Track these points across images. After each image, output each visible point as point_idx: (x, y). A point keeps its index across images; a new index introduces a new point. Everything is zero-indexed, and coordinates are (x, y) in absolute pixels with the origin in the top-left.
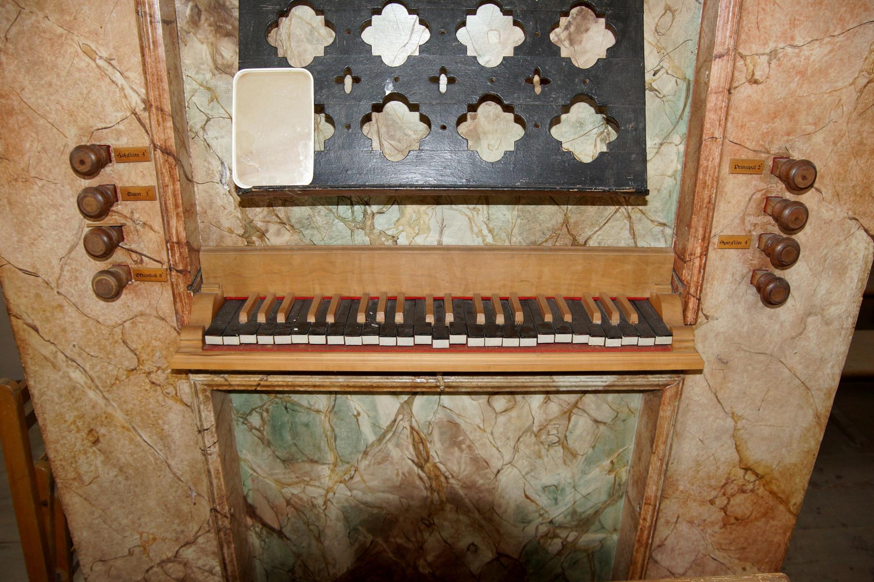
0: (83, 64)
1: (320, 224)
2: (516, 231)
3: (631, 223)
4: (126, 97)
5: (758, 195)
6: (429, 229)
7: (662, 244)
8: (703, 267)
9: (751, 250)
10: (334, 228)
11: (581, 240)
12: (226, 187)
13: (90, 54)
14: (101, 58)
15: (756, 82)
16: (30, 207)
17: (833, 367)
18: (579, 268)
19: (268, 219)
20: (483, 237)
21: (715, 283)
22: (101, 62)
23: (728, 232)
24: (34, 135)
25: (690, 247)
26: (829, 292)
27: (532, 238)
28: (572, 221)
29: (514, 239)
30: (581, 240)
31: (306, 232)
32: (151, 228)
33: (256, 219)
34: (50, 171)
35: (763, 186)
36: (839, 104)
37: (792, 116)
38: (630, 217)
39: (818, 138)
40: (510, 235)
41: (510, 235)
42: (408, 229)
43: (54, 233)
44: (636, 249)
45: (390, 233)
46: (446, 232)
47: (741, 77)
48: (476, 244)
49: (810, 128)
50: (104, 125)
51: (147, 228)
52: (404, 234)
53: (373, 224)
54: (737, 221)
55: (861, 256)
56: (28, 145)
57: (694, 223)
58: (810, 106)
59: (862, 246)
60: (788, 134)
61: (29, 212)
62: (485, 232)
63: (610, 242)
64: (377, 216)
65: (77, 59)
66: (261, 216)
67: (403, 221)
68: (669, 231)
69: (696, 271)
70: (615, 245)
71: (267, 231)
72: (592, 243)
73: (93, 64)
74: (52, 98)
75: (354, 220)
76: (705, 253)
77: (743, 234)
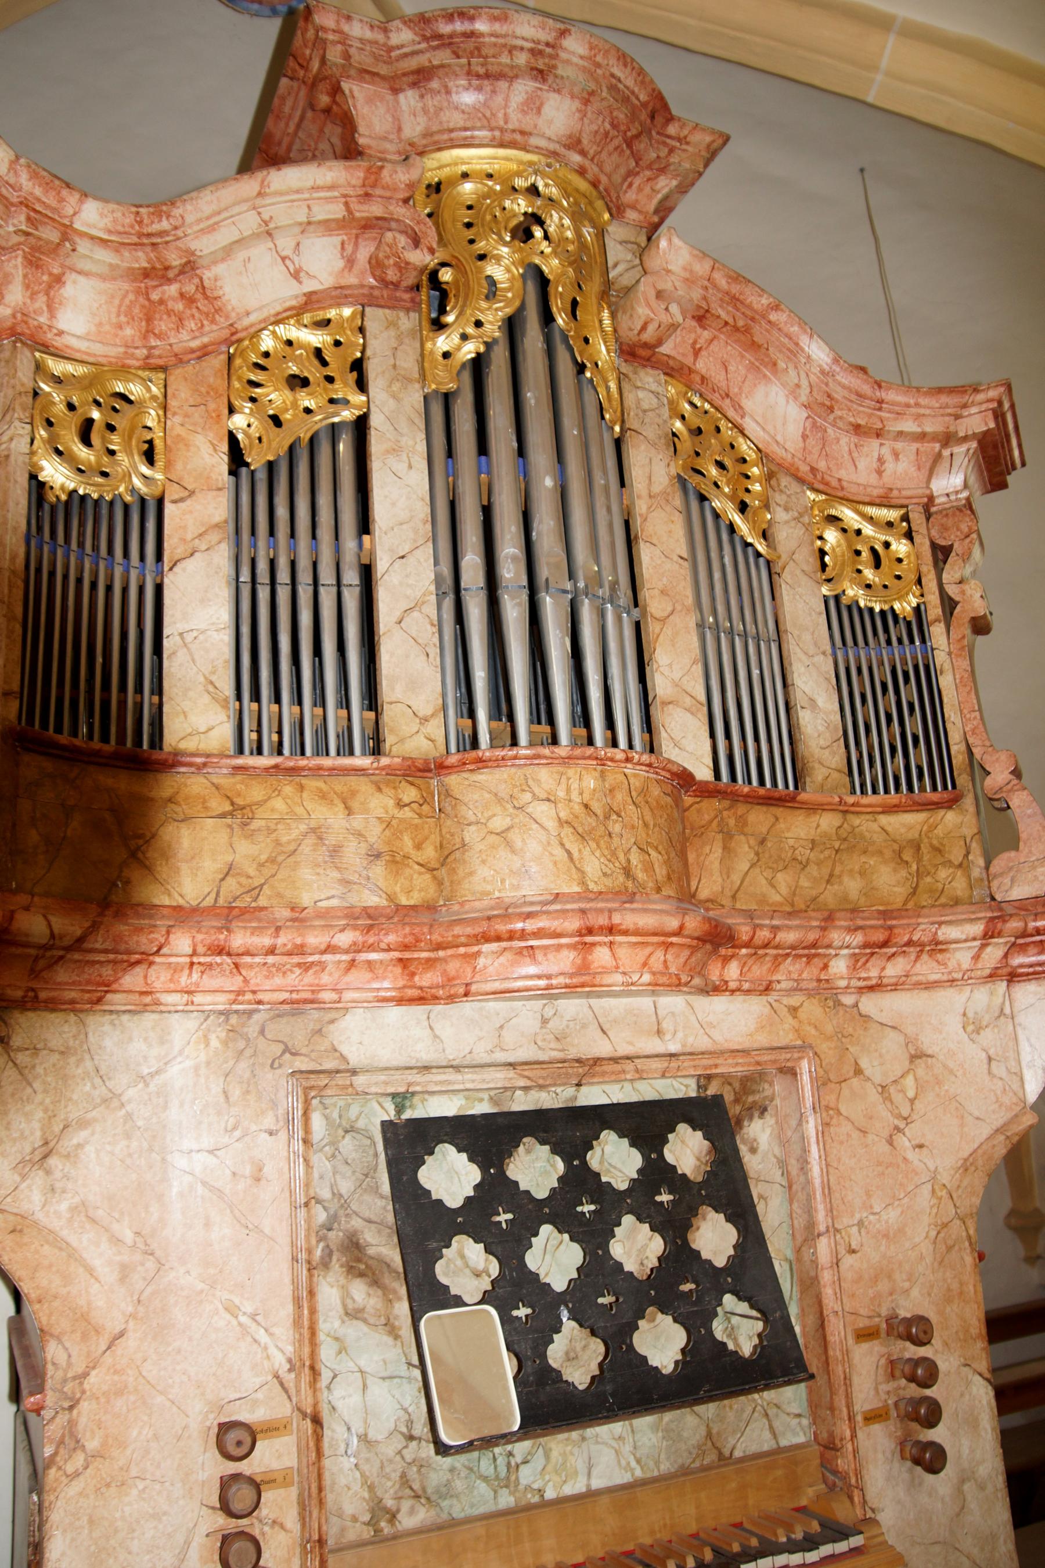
0: (222, 1323)
1: (460, 1489)
2: (663, 1456)
3: (769, 1421)
4: (268, 1357)
5: (883, 1361)
6: (576, 1473)
7: (801, 1439)
8: (855, 1451)
9: (891, 1422)
10: (476, 1493)
11: (727, 1453)
12: (352, 1459)
13: (232, 1310)
14: (245, 1313)
15: (854, 1252)
16: (119, 1523)
17: (1005, 1542)
18: (734, 1485)
19: (400, 1494)
20: (632, 1470)
21: (871, 1467)
22: (243, 1319)
23: (867, 1407)
24: (146, 1418)
25: (837, 1432)
26: (972, 1451)
27: (680, 1461)
28: (714, 1431)
29: (662, 1467)
30: (727, 1453)
31: (445, 1504)
32: (282, 1527)
33: (387, 1496)
34: (158, 1466)
35: (884, 1350)
36: (922, 1258)
37: (889, 1277)
38: (767, 1415)
39: (915, 1293)
40: (657, 1463)
41: (657, 1463)
42: (556, 1478)
43: (147, 1557)
44: (779, 1450)
45: (535, 1486)
46: (595, 1472)
47: (842, 1251)
48: (625, 1481)
49: (906, 1285)
50: (238, 1396)
51: (277, 1528)
52: (551, 1484)
53: (517, 1479)
54: (872, 1392)
55: (985, 1402)
56: (135, 1433)
57: (836, 1403)
58: (900, 1264)
59: (982, 1391)
60: (891, 1294)
61: (116, 1531)
62: (633, 1464)
63: (754, 1448)
64: (522, 1467)
65: (216, 1318)
66: (392, 1491)
67: (549, 1468)
68: (805, 1422)
69: (851, 1457)
70: (759, 1451)
71: (398, 1511)
72: (738, 1454)
73: (235, 1322)
74: (178, 1368)
75: (497, 1478)
76: (854, 1436)
77: (881, 1405)
